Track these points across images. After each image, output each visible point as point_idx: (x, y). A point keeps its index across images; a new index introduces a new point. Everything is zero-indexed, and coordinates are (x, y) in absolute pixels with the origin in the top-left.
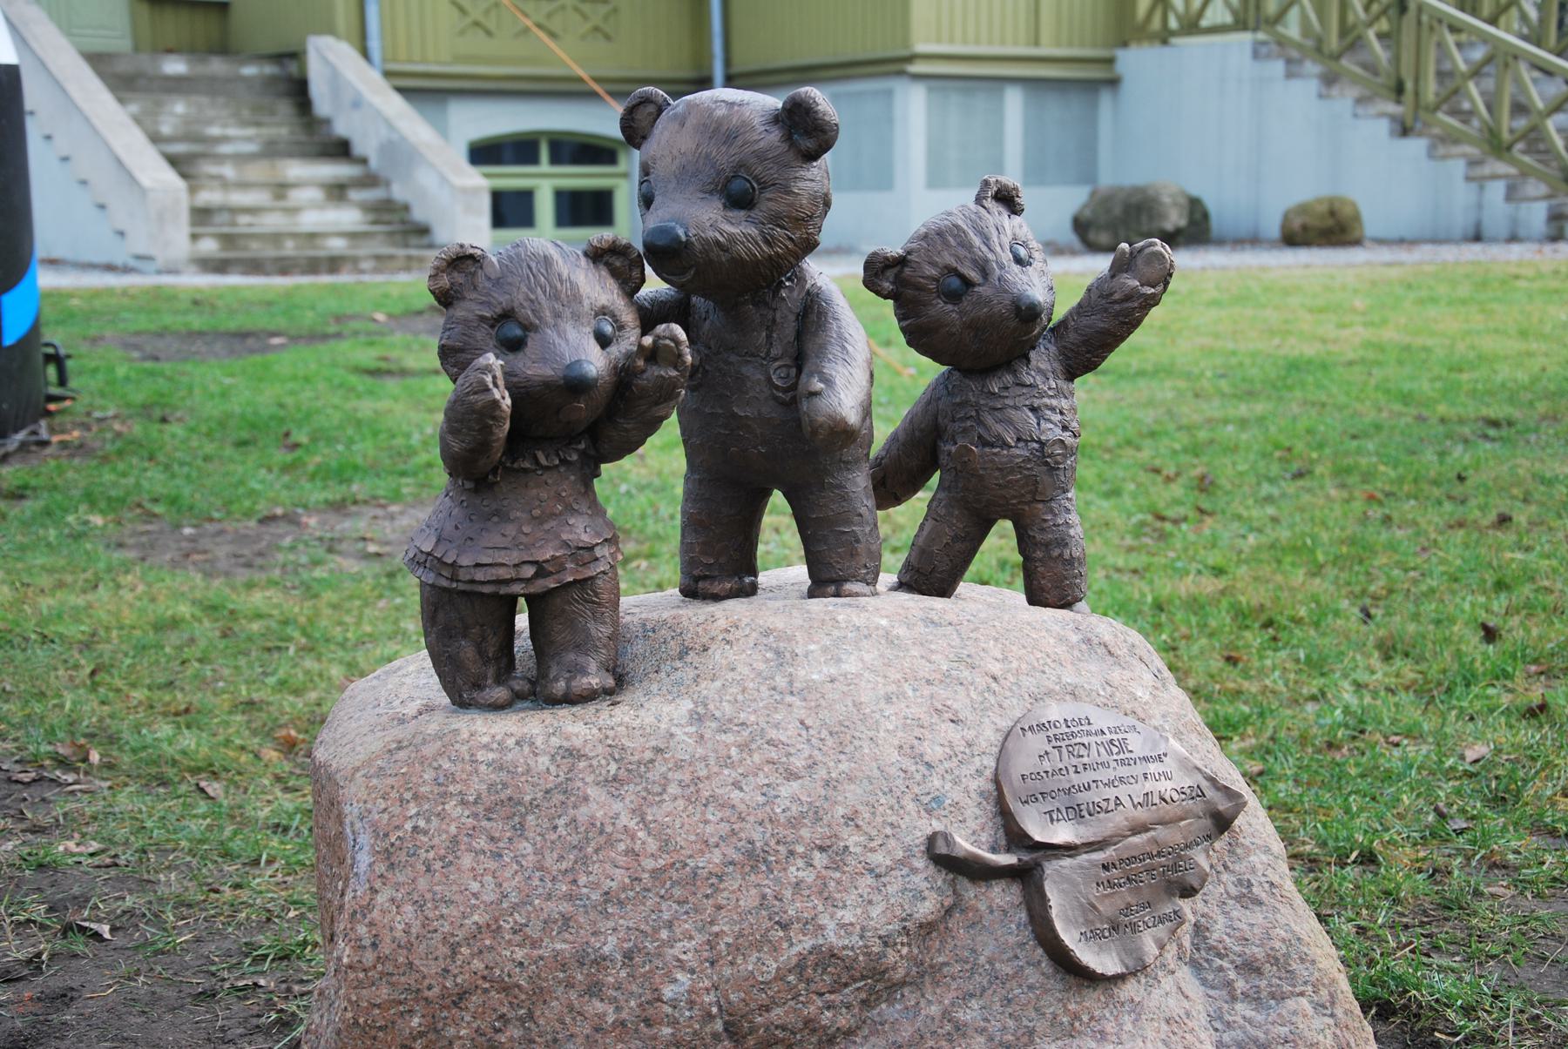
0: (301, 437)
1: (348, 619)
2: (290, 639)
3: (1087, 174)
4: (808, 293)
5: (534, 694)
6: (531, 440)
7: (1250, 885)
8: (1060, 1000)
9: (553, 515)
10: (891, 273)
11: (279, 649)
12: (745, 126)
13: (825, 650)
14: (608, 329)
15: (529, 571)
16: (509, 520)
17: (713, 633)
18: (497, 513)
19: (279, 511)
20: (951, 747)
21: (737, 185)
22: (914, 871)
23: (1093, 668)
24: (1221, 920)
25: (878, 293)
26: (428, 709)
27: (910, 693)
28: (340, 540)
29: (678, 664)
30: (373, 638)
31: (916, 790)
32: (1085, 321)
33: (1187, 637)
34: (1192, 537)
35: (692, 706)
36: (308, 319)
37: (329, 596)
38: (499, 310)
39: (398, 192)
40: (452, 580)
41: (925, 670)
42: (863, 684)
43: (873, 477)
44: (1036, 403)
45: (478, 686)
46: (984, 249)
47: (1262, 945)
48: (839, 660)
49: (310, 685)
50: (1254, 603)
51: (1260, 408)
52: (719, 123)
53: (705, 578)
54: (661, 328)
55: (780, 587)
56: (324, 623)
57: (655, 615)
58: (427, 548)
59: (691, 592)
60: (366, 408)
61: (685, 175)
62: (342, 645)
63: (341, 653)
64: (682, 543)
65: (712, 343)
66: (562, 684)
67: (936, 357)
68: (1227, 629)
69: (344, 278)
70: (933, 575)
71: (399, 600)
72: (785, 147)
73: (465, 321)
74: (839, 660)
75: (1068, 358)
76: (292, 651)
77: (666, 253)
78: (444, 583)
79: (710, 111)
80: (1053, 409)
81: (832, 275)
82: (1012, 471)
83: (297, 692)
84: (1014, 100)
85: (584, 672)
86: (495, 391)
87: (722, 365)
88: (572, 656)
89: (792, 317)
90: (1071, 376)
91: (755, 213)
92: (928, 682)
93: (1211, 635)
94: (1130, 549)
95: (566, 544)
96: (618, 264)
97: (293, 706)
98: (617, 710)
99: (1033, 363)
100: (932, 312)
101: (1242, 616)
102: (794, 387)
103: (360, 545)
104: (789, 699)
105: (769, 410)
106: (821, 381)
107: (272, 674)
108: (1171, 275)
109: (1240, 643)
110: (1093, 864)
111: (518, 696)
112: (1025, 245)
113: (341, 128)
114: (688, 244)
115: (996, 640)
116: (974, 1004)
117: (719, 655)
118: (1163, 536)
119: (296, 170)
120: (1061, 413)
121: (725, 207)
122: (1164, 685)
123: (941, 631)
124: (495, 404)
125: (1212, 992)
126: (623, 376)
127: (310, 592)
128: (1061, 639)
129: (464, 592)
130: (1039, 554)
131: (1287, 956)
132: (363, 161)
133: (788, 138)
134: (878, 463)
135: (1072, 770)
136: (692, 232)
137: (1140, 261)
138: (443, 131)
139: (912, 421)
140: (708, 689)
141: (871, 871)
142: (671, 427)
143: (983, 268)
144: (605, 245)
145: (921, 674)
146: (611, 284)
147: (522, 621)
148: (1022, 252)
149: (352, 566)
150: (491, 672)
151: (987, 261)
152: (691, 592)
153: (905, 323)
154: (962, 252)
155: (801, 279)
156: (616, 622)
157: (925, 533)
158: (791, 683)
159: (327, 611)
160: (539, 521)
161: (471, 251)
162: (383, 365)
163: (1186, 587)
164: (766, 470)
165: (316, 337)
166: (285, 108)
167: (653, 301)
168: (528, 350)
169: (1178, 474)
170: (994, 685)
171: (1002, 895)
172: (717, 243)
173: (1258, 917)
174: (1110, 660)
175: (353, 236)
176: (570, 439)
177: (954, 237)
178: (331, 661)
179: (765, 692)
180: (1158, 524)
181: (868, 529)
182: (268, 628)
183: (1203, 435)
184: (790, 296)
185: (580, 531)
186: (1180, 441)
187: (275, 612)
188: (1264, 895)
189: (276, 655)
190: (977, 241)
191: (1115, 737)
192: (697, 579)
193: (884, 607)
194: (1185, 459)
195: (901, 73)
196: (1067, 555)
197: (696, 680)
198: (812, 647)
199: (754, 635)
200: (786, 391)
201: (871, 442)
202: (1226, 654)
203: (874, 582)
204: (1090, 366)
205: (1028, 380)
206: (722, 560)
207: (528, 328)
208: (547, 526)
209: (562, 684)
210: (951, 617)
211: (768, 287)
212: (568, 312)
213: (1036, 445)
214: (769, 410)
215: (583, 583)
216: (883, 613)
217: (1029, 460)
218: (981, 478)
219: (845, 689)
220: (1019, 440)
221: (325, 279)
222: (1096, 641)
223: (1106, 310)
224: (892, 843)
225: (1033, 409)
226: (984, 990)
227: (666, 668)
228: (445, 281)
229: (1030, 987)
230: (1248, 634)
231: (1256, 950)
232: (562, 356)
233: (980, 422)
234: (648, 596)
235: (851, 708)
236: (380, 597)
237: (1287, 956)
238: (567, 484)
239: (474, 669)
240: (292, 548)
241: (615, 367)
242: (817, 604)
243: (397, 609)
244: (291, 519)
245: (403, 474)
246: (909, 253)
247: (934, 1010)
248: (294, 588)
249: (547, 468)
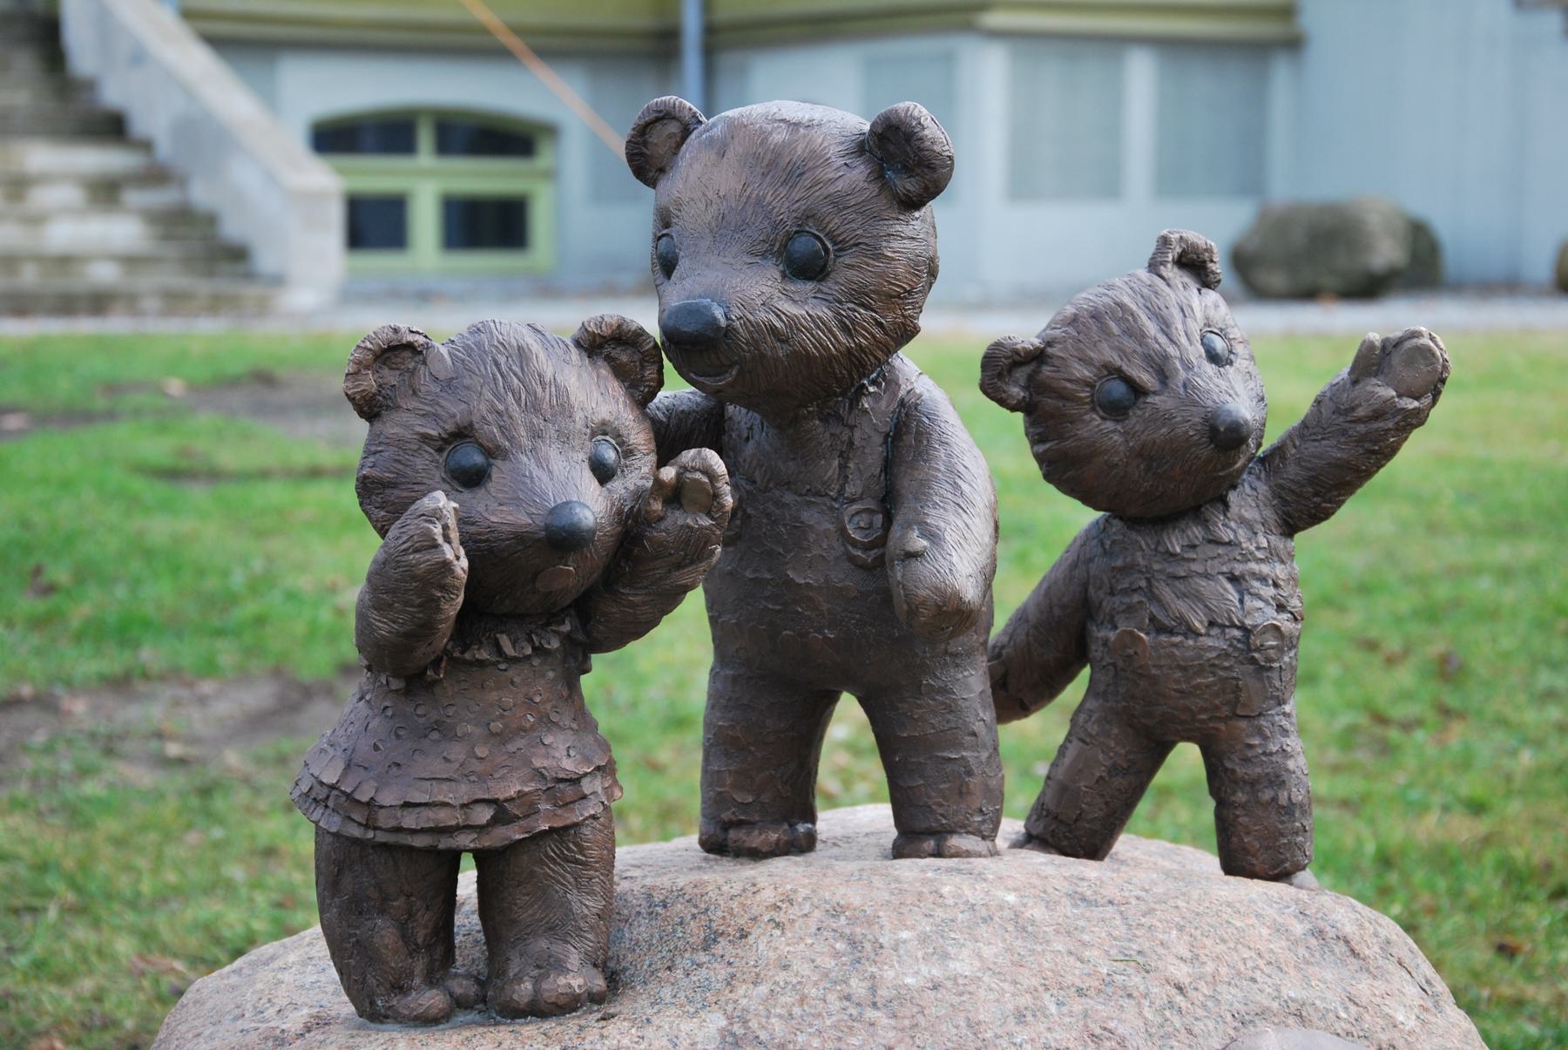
0: (59, 573)
1: (142, 863)
2: (49, 894)
3: (1251, 182)
4: (902, 403)
5: (484, 1000)
6: (493, 615)
9: (522, 730)
10: (1021, 374)
11: (34, 910)
12: (816, 158)
13: (924, 939)
14: (610, 455)
15: (484, 815)
16: (455, 738)
17: (755, 911)
18: (437, 726)
19: (26, 690)
21: (802, 245)
23: (1329, 976)
25: (1002, 402)
26: (320, 1022)
27: (1053, 1008)
28: (122, 737)
29: (702, 957)
30: (179, 893)
32: (1311, 448)
33: (1433, 911)
34: (1431, 751)
35: (723, 1023)
36: (63, 388)
37: (111, 825)
38: (450, 427)
39: (201, 194)
40: (367, 827)
41: (1074, 974)
42: (982, 993)
43: (992, 672)
44: (1238, 569)
45: (399, 988)
46: (1163, 339)
48: (945, 956)
49: (82, 968)
50: (1536, 859)
51: (1531, 550)
52: (777, 153)
53: (739, 824)
54: (688, 456)
55: (847, 839)
56: (102, 868)
57: (665, 881)
58: (330, 777)
59: (716, 846)
60: (160, 529)
61: (726, 229)
62: (133, 904)
63: (130, 917)
64: (705, 771)
65: (757, 476)
66: (527, 986)
67: (1088, 499)
68: (1494, 901)
69: (116, 325)
70: (1078, 824)
71: (217, 833)
72: (873, 189)
73: (399, 442)
74: (945, 956)
75: (1285, 502)
76: (52, 914)
77: (694, 344)
78: (356, 832)
79: (764, 136)
80: (1263, 579)
81: (935, 367)
82: (1200, 671)
83: (62, 979)
84: (1141, 75)
85: (560, 967)
86: (446, 547)
87: (771, 507)
88: (543, 944)
89: (878, 439)
90: (1290, 527)
91: (831, 287)
92: (1081, 992)
93: (1471, 908)
94: (1336, 769)
95: (539, 774)
96: (624, 358)
97: (56, 1001)
98: (612, 1028)
99: (1234, 509)
100: (1083, 432)
101: (1516, 878)
102: (882, 541)
103: (154, 745)
104: (870, 1014)
105: (843, 577)
106: (923, 535)
107: (23, 950)
108: (1443, 381)
109: (1517, 923)
111: (460, 1004)
112: (1222, 334)
113: (113, 94)
114: (729, 332)
115: (1181, 929)
117: (764, 945)
118: (1385, 749)
119: (40, 157)
120: (1276, 585)
121: (784, 276)
122: (1436, 1004)
123: (1096, 913)
124: (446, 566)
126: (632, 526)
127: (76, 816)
128: (1280, 930)
129: (385, 846)
130: (1241, 797)
132: (146, 146)
133: (879, 176)
134: (996, 655)
136: (736, 313)
137: (1396, 359)
138: (269, 99)
139: (1048, 594)
140: (749, 996)
142: (694, 603)
143: (1161, 368)
144: (606, 331)
145: (1069, 979)
146: (615, 388)
147: (467, 882)
148: (1219, 344)
149: (145, 777)
150: (420, 965)
151: (1166, 357)
152: (716, 846)
153: (1041, 448)
154: (1129, 344)
155: (892, 383)
156: (608, 893)
157: (1067, 761)
158: (873, 989)
159: (108, 850)
160: (501, 738)
161: (411, 338)
162: (184, 464)
163: (1429, 827)
164: (833, 661)
165: (74, 416)
166: (25, 62)
167: (670, 411)
168: (492, 486)
169: (1406, 652)
170: (1179, 998)
172: (773, 330)
174: (1354, 963)
175: (131, 261)
176: (551, 617)
177: (1118, 321)
178: (116, 929)
179: (835, 1004)
180: (1378, 730)
181: (984, 755)
182: (14, 878)
183: (1442, 591)
184: (875, 407)
185: (561, 754)
186: (1407, 601)
187: (24, 851)
189: (27, 920)
190: (1151, 328)
192: (727, 826)
193: (1008, 876)
194: (1417, 629)
195: (969, 28)
196: (1283, 798)
197: (730, 981)
198: (905, 935)
199: (817, 914)
200: (866, 547)
201: (990, 625)
202: (1497, 939)
203: (990, 835)
204: (1318, 515)
205: (1227, 535)
206: (766, 798)
207: (492, 452)
208: (511, 748)
209: (527, 986)
210: (1111, 892)
211: (843, 394)
212: (551, 430)
213: (1237, 633)
214: (843, 577)
215: (559, 833)
216: (1010, 883)
217: (1227, 655)
218: (1154, 680)
219: (956, 1000)
220: (1212, 624)
221: (85, 326)
222: (1331, 933)
223: (1344, 432)
225: (1234, 579)
227: (683, 962)
228: (370, 382)
230: (1530, 911)
232: (543, 496)
233: (1154, 598)
234: (655, 855)
235: (964, 1031)
236: (189, 826)
238: (542, 684)
239: (394, 963)
240: (48, 749)
241: (619, 512)
242: (909, 869)
243: (217, 845)
244: (45, 703)
245: (220, 633)
246: (1049, 344)
248: (52, 811)
249: (514, 660)
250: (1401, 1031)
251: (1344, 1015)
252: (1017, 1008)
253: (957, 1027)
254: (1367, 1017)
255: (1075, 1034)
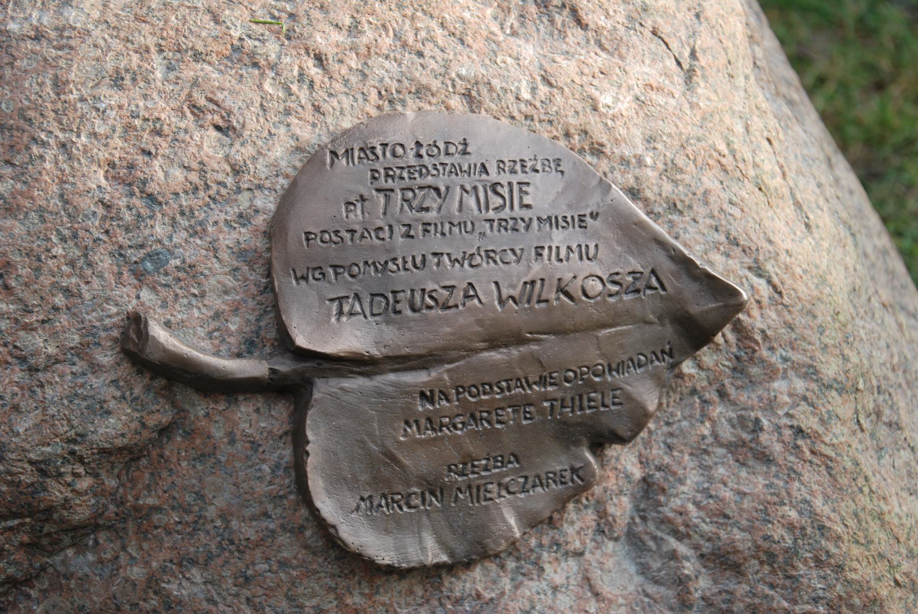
7: (757, 428)
8: (330, 590)
20: (202, 172)
22: (95, 368)
24: (693, 478)
31: (122, 238)
47: (749, 530)
110: (404, 391)
116: (196, 574)
125: (651, 589)
131: (791, 553)
135: (400, 230)
141: (23, 359)
171: (253, 419)
173: (757, 482)
188: (778, 448)
191: (504, 179)
224: (64, 319)
226: (210, 557)
229: (284, 564)
231: (738, 535)
237: (791, 553)
247: (137, 572)
250: (602, 115)
251: (526, 95)
252: (117, 70)
253: (41, 85)
254: (559, 98)
255: (173, 103)
